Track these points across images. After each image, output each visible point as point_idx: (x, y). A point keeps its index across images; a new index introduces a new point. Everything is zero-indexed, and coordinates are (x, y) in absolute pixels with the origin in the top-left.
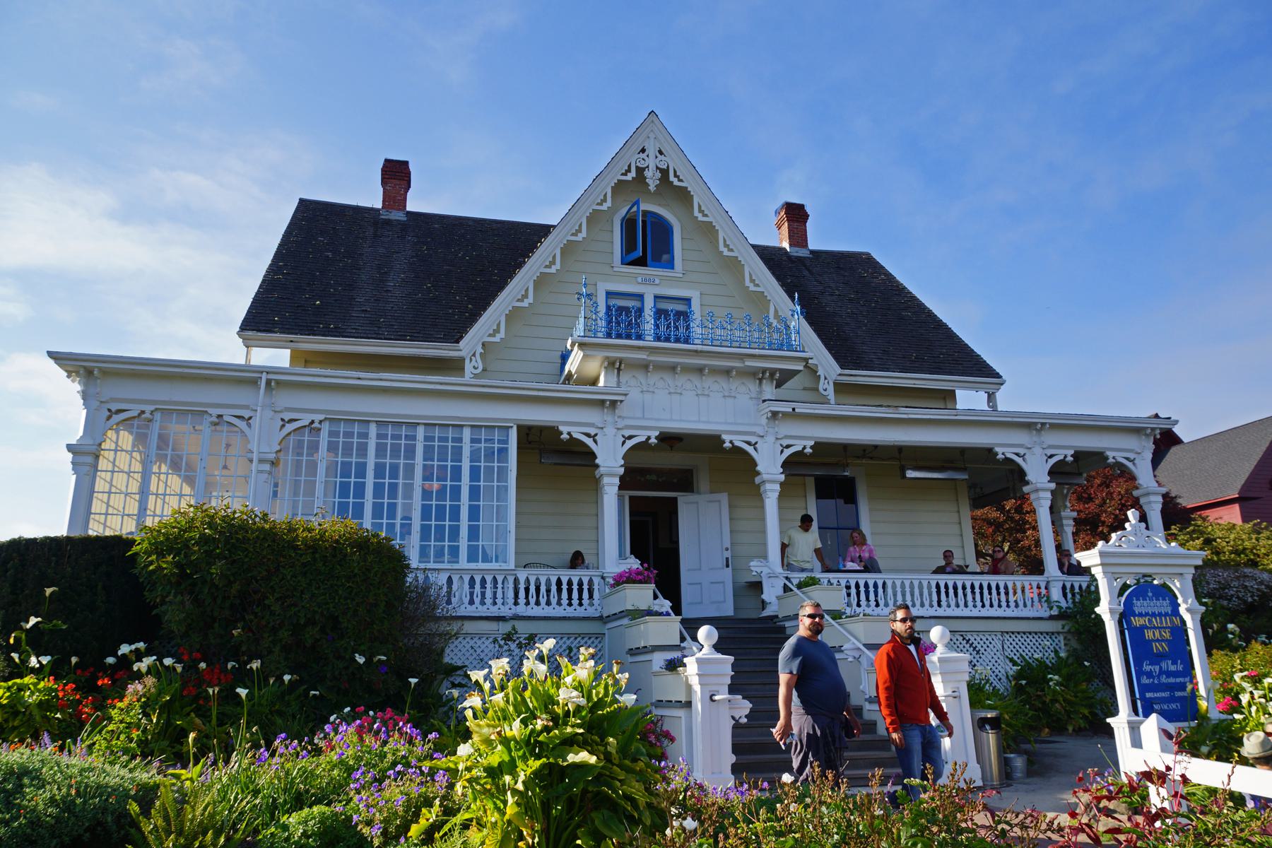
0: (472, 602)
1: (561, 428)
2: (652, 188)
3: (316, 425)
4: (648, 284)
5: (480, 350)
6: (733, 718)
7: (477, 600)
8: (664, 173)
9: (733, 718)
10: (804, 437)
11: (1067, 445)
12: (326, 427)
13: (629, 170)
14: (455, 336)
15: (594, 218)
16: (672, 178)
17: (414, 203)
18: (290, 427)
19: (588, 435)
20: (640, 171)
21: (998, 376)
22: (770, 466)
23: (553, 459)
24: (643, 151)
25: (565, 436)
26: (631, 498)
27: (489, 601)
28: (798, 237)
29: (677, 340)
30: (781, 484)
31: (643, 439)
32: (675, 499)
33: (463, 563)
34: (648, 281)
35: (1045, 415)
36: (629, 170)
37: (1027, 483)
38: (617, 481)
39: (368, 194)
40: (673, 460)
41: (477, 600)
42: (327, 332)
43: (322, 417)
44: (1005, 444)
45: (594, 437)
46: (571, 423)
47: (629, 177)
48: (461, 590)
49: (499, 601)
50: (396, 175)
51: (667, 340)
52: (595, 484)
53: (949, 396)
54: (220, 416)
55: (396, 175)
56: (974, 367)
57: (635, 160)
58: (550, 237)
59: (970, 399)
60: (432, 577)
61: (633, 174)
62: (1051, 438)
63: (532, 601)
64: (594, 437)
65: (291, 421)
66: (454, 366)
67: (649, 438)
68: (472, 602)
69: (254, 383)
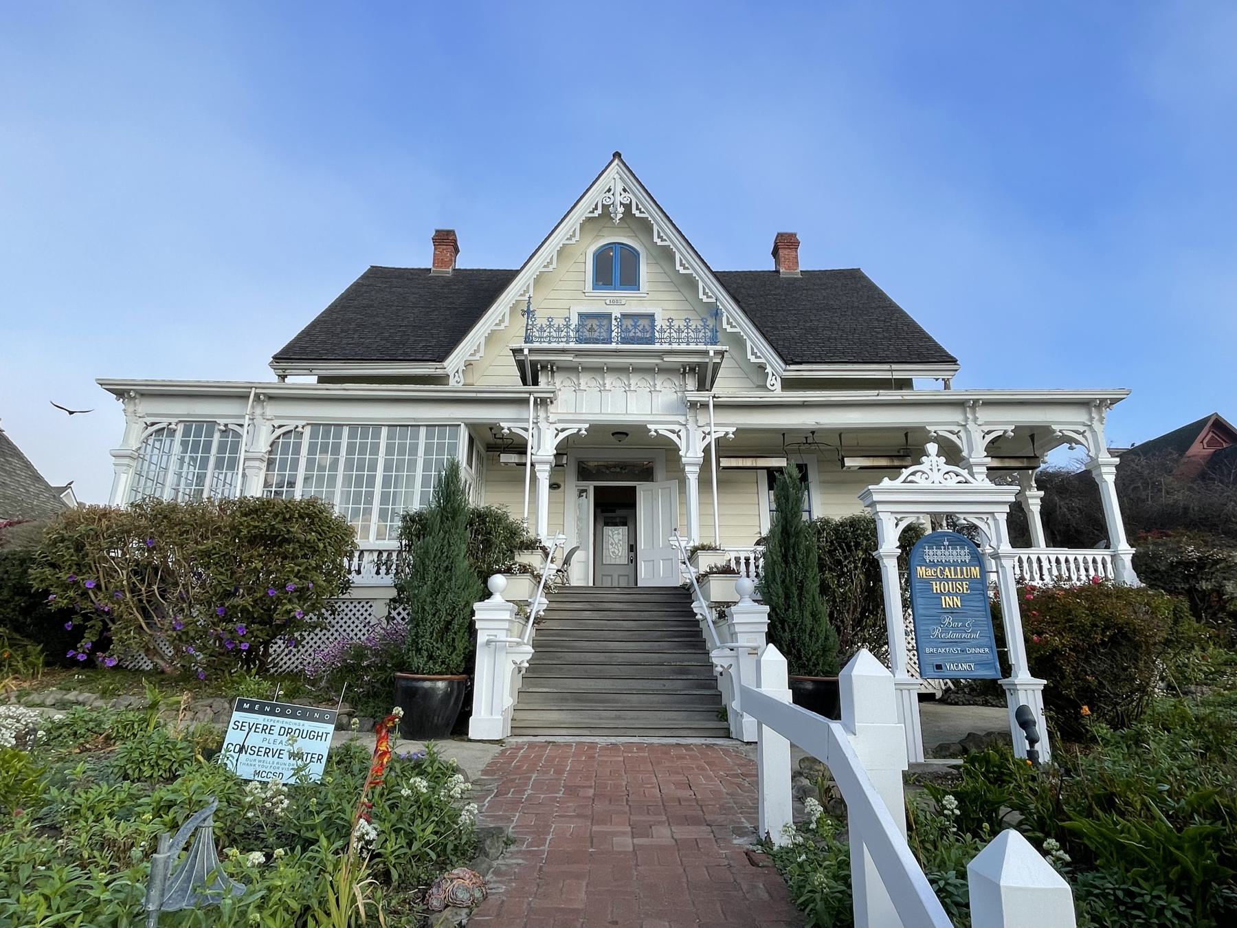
1: (502, 424)
3: (300, 429)
6: (515, 663)
8: (628, 207)
9: (515, 663)
10: (724, 425)
11: (1005, 421)
12: (307, 431)
13: (596, 208)
14: (441, 358)
16: (634, 211)
17: (464, 262)
18: (151, 429)
19: (673, 432)
22: (692, 453)
24: (609, 190)
30: (1117, 467)
31: (1001, 433)
36: (596, 208)
39: (420, 257)
43: (304, 423)
45: (678, 433)
47: (596, 214)
50: (445, 240)
54: (226, 425)
55: (445, 240)
56: (929, 353)
59: (925, 381)
61: (599, 211)
62: (984, 415)
64: (678, 433)
65: (280, 427)
67: (580, 430)
69: (245, 397)
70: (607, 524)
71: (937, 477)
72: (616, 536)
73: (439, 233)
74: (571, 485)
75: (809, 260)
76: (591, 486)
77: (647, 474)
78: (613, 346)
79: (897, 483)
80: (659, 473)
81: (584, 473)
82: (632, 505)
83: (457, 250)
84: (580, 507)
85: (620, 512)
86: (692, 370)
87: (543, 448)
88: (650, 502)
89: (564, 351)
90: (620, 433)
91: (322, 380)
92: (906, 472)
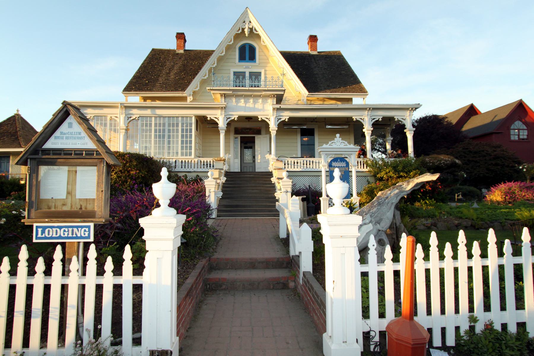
0: (182, 167)
2: (247, 35)
4: (247, 68)
5: (192, 93)
7: (183, 167)
11: (379, 115)
13: (239, 30)
14: (184, 89)
15: (229, 48)
17: (189, 46)
20: (243, 29)
21: (366, 92)
22: (273, 127)
23: (206, 125)
24: (244, 22)
25: (354, 120)
26: (241, 137)
27: (186, 167)
28: (314, 48)
29: (243, 86)
32: (254, 137)
33: (179, 156)
34: (247, 67)
35: (370, 105)
36: (239, 30)
37: (406, 128)
38: (224, 131)
39: (171, 44)
40: (248, 125)
41: (183, 167)
42: (147, 90)
44: (355, 116)
46: (210, 114)
48: (179, 164)
49: (190, 167)
51: (239, 86)
52: (218, 133)
53: (350, 100)
55: (181, 37)
57: (241, 26)
58: (213, 55)
59: (357, 101)
60: (171, 160)
61: (241, 31)
63: (199, 167)
66: (184, 99)
68: (182, 167)
70: (246, 148)
71: (338, 144)
72: (248, 153)
73: (178, 34)
74: (232, 136)
75: (323, 46)
76: (239, 136)
77: (259, 132)
78: (247, 88)
79: (328, 146)
80: (263, 131)
81: (237, 131)
82: (254, 142)
83: (185, 41)
84: (235, 143)
85: (249, 145)
86: (274, 96)
87: (222, 124)
88: (260, 142)
89: (230, 90)
90: (249, 119)
91: (145, 99)
92: (330, 143)
